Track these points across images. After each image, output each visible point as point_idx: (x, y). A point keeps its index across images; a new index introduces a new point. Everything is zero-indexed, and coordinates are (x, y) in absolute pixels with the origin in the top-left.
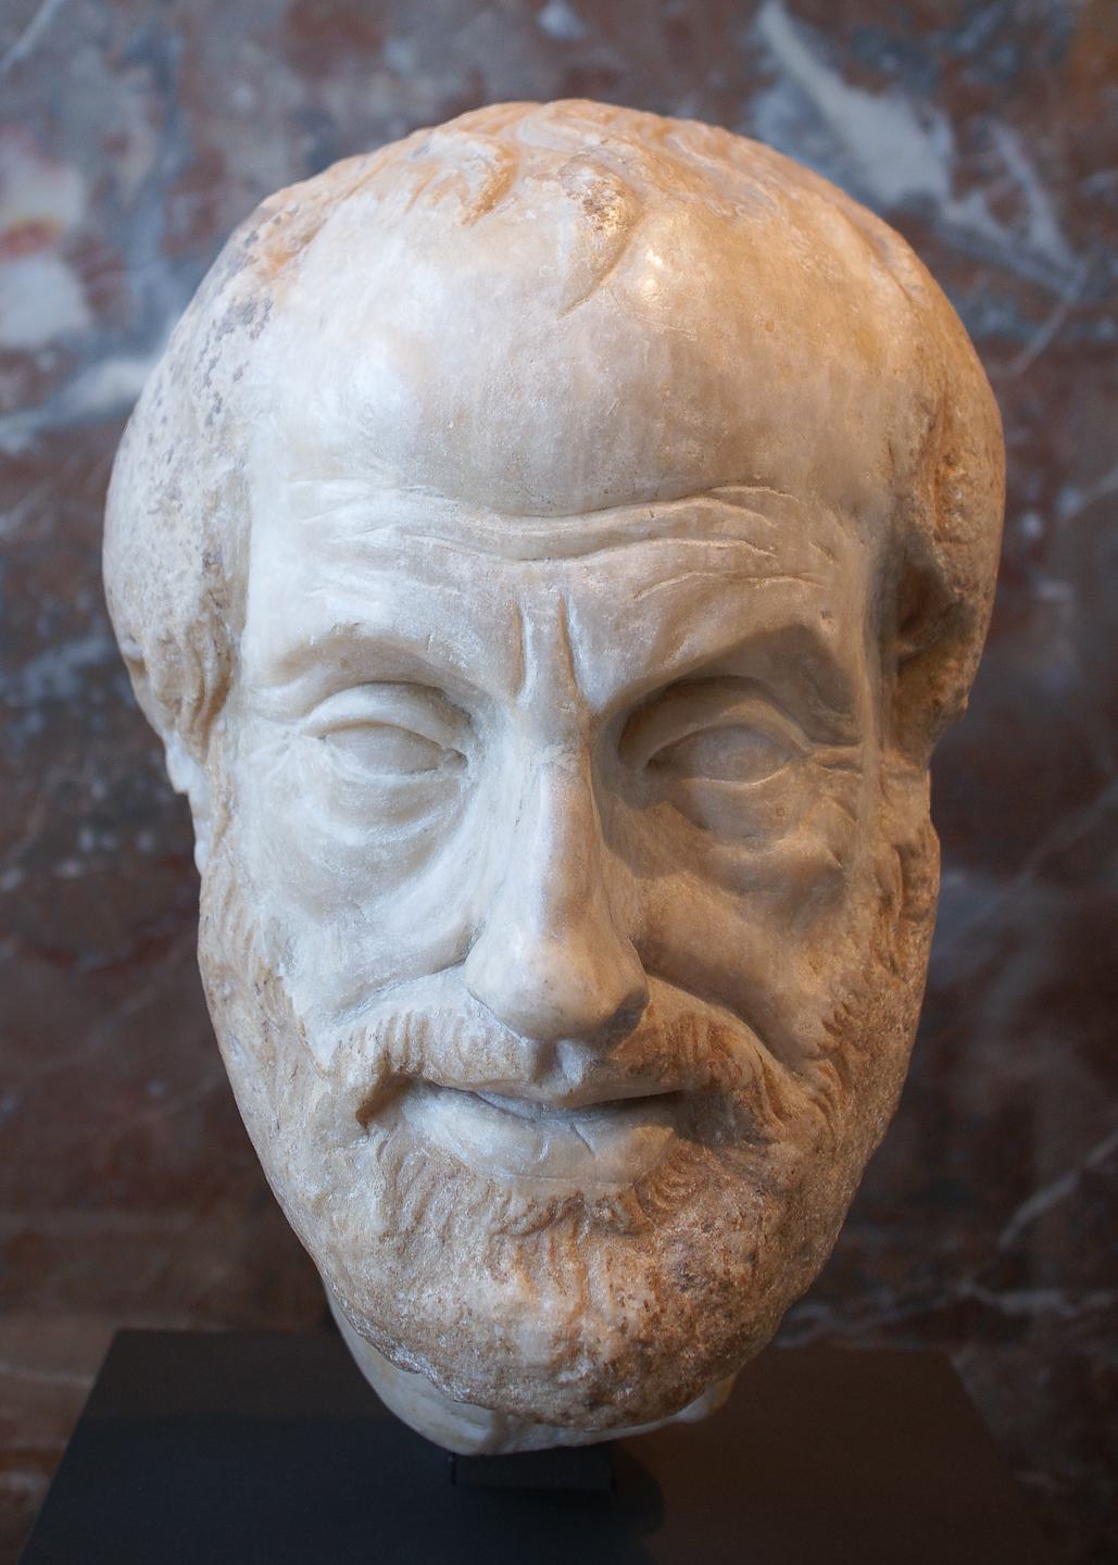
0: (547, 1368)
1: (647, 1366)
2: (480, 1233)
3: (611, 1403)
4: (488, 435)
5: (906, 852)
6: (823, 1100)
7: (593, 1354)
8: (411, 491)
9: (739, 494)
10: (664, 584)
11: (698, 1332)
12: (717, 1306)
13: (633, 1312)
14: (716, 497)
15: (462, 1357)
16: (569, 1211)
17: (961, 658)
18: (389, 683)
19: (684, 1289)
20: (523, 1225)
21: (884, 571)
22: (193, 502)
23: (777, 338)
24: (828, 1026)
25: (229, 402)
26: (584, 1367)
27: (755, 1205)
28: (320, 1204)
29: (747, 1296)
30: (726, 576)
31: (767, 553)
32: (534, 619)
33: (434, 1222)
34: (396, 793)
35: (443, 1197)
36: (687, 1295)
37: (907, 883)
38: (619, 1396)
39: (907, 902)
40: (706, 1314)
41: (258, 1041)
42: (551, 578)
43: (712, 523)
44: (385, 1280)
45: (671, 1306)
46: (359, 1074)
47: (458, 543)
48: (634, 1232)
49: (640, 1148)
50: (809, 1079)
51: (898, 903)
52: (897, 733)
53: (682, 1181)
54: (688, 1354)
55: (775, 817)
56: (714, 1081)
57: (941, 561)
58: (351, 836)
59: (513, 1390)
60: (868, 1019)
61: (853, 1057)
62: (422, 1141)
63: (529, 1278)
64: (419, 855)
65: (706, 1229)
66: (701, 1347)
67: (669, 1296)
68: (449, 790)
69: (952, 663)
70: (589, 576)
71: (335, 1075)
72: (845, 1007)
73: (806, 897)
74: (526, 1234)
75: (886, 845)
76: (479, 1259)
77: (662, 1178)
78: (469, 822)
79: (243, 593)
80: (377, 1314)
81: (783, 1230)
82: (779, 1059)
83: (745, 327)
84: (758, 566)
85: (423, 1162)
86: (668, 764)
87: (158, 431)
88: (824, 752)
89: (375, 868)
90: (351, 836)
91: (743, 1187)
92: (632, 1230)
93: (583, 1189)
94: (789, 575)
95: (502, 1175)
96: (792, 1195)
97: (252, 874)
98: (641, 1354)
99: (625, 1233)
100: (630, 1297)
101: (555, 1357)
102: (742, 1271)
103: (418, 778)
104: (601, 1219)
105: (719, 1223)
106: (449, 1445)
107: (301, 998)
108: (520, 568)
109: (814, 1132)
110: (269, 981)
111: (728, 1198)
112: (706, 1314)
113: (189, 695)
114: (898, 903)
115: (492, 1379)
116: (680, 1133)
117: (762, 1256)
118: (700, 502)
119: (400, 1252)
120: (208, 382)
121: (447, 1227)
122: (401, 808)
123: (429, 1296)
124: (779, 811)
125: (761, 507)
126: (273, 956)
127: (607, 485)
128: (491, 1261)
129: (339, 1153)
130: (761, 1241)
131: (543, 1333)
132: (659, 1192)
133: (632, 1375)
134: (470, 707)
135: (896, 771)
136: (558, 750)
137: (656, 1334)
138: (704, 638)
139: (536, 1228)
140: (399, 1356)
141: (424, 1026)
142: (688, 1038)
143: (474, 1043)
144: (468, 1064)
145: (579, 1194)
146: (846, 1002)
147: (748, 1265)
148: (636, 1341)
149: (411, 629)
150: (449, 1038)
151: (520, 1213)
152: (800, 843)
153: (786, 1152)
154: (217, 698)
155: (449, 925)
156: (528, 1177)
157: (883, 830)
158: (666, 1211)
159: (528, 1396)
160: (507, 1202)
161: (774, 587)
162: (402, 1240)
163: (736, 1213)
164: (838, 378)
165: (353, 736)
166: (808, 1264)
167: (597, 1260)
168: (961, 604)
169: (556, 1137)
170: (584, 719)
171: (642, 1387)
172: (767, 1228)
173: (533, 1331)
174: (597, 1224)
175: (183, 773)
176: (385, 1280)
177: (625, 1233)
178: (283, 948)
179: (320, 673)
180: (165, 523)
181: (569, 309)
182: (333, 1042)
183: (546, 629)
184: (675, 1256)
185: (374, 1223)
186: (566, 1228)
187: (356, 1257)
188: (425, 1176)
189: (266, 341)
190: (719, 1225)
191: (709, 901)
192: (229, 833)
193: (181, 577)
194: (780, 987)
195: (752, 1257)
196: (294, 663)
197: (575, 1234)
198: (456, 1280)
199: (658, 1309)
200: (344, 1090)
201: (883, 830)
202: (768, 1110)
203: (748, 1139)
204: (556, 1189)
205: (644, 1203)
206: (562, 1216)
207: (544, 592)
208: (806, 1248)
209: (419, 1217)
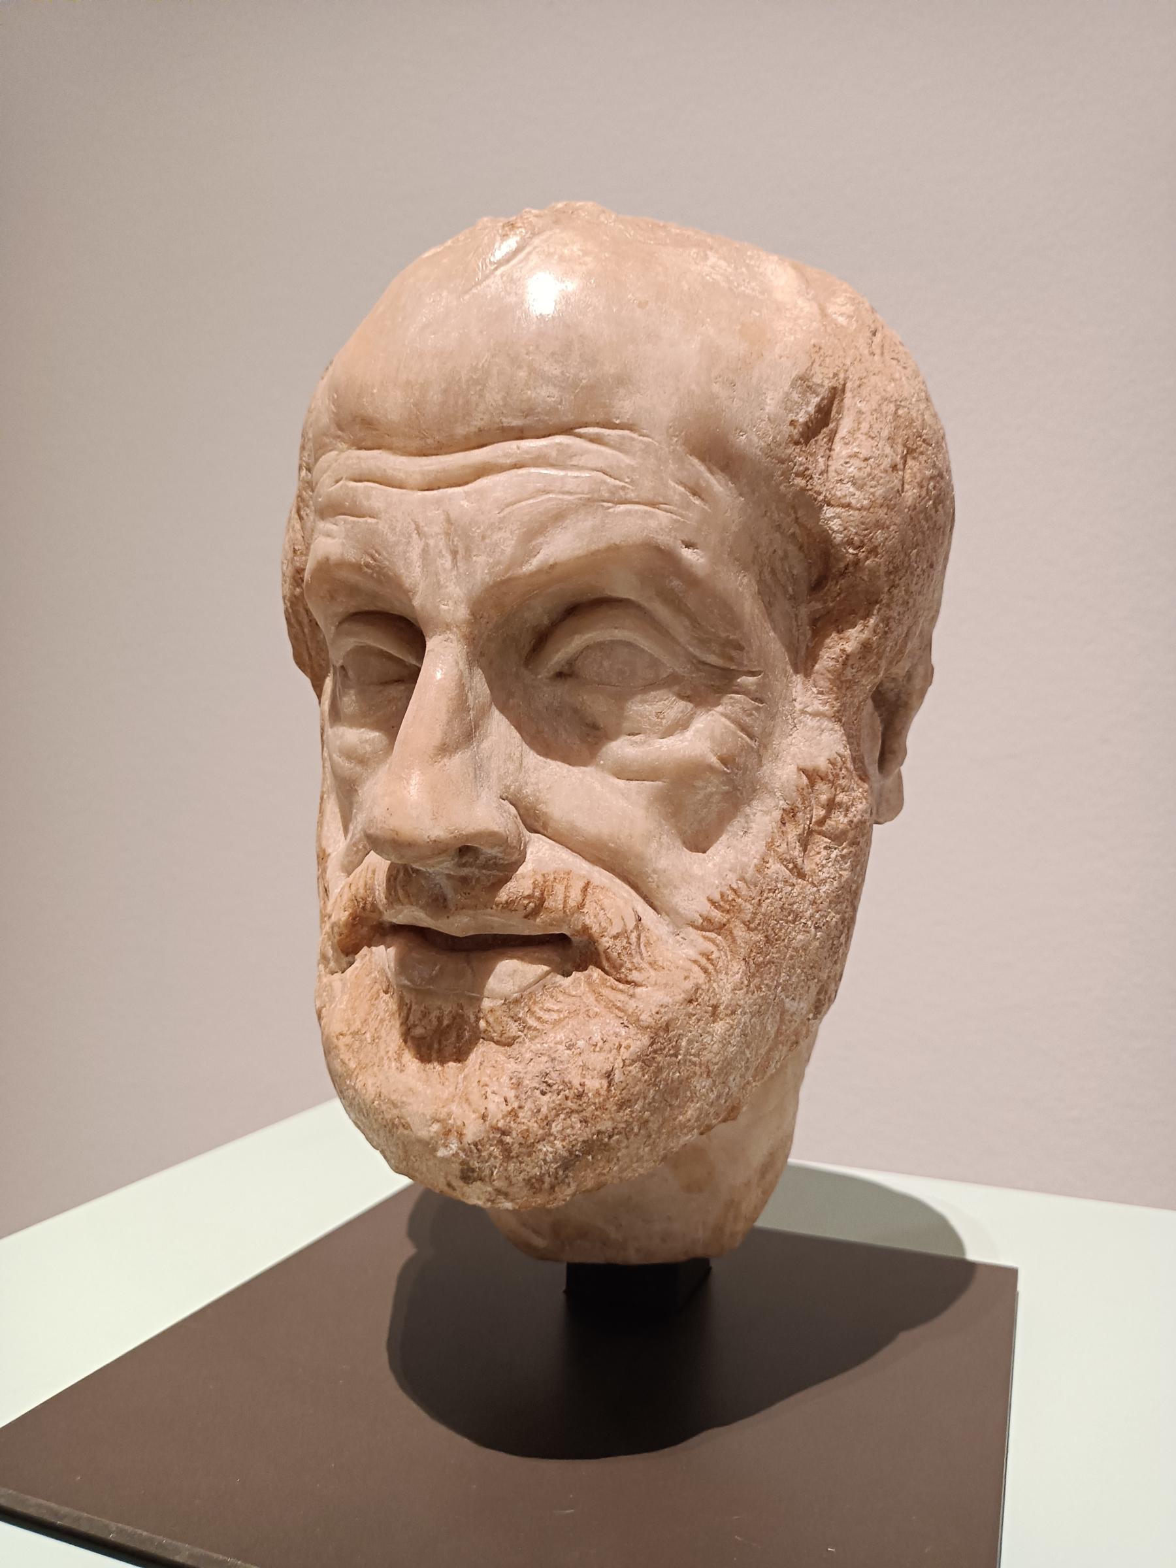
7: (461, 1135)
12: (572, 1111)
14: (580, 436)
19: (543, 1093)
27: (617, 1035)
31: (622, 484)
36: (545, 1098)
45: (529, 1105)
54: (545, 1148)
55: (655, 719)
60: (759, 904)
65: (568, 1048)
66: (558, 1144)
67: (529, 1097)
75: (793, 768)
77: (535, 1003)
84: (613, 493)
92: (503, 1039)
98: (501, 1142)
100: (494, 1093)
102: (597, 1085)
109: (688, 985)
112: (562, 1116)
117: (618, 1076)
125: (619, 447)
130: (619, 1064)
146: (735, 886)
147: (605, 1083)
158: (536, 1029)
161: (629, 513)
163: (597, 1038)
191: (597, 786)
199: (516, 1105)
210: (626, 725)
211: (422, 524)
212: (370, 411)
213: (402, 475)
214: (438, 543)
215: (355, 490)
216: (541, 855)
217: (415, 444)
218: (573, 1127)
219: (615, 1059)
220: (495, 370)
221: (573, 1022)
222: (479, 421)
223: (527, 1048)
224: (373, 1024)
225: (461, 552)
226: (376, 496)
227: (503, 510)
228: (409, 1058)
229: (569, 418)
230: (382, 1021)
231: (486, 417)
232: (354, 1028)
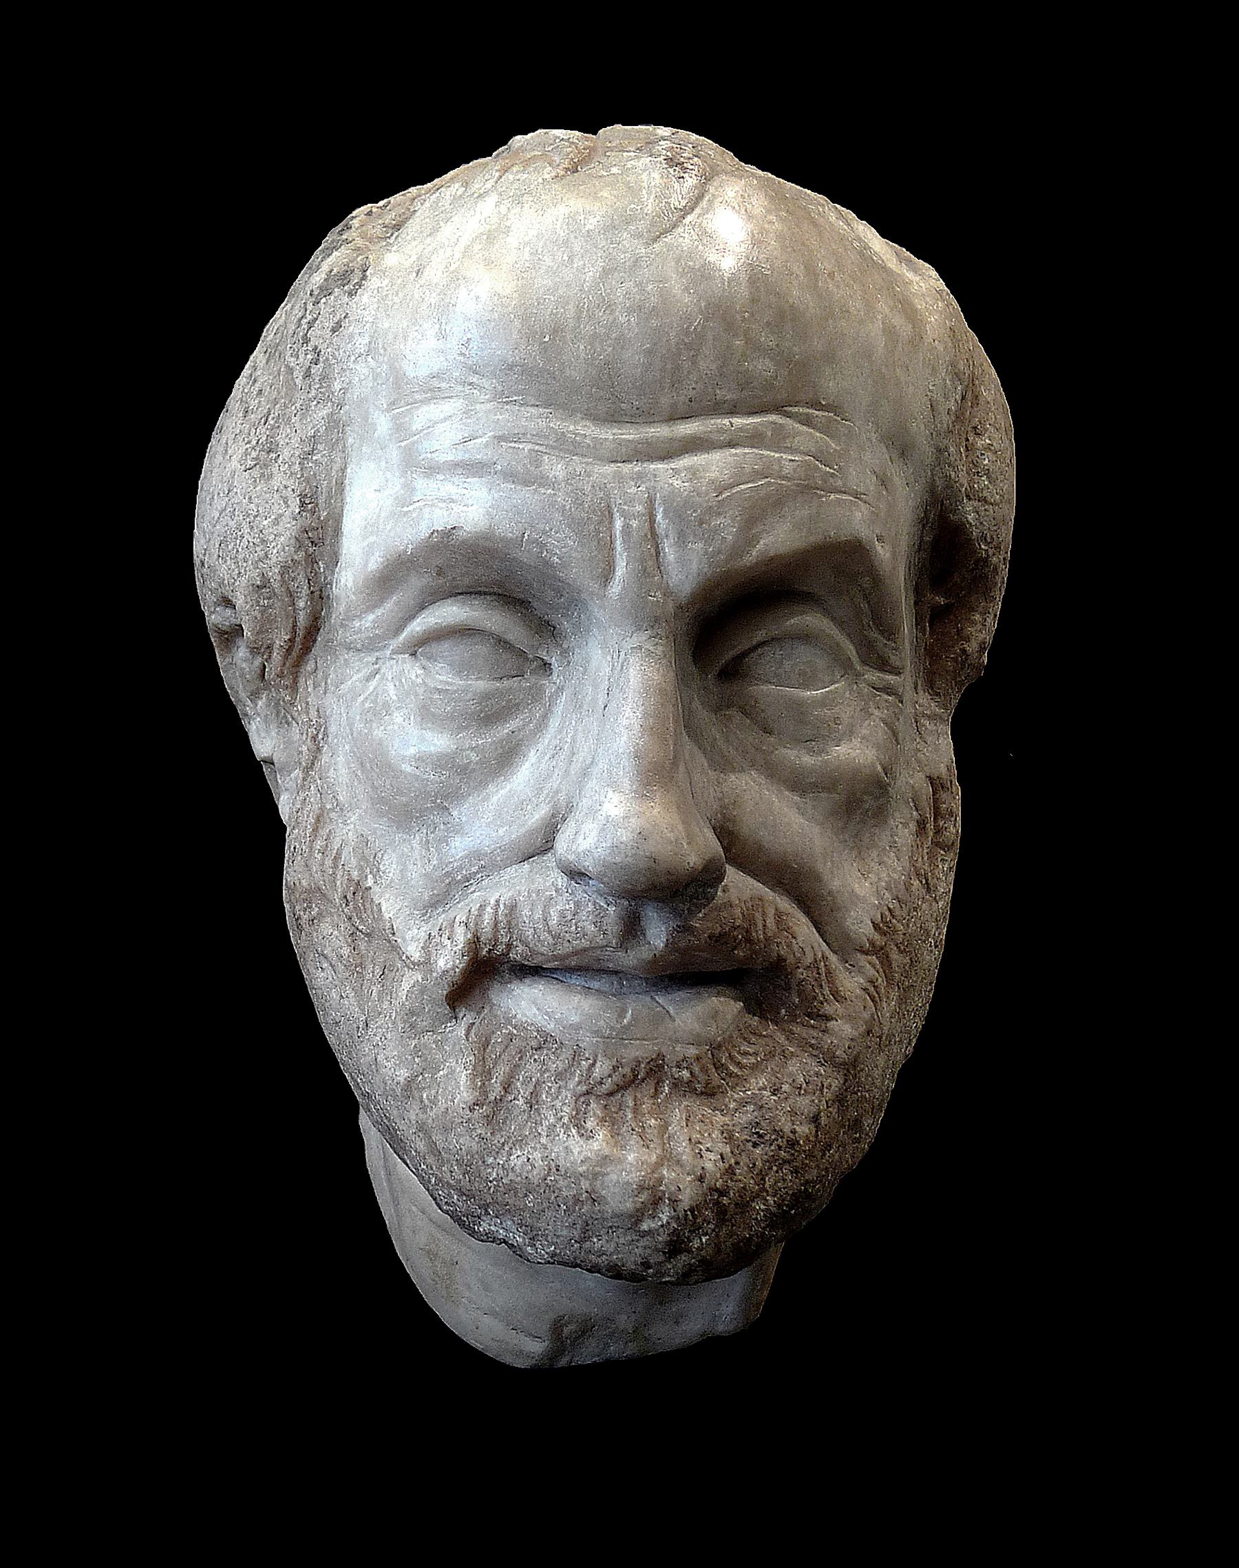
0: (632, 1216)
1: (722, 1213)
2: (567, 1095)
3: (689, 1251)
4: (582, 347)
5: (936, 783)
6: (873, 994)
7: (674, 1202)
8: (507, 403)
9: (807, 414)
10: (743, 487)
11: (767, 1185)
12: (785, 1162)
13: (710, 1163)
14: (788, 415)
15: (549, 1214)
16: (650, 1073)
17: (985, 613)
18: (479, 593)
19: (755, 1145)
20: (608, 1085)
21: (923, 522)
22: (290, 445)
23: (838, 287)
24: (876, 926)
25: (326, 351)
26: (665, 1216)
27: (817, 1074)
28: (410, 1087)
29: (810, 1155)
30: (798, 485)
32: (624, 514)
33: (522, 1091)
34: (486, 696)
35: (531, 1068)
37: (937, 814)
38: (696, 1244)
39: (938, 831)
40: (775, 1168)
41: (346, 951)
42: (639, 478)
43: (784, 438)
44: (475, 1147)
45: (744, 1159)
46: (450, 959)
47: (553, 448)
48: (709, 1093)
49: (715, 1015)
50: (861, 971)
51: (930, 826)
52: (930, 682)
53: (751, 1051)
56: (781, 959)
57: (971, 517)
58: (439, 742)
59: (596, 1243)
61: (895, 956)
62: (508, 1021)
63: (615, 1134)
64: (506, 757)
68: (536, 694)
69: (977, 617)
70: (670, 476)
71: (426, 964)
72: (889, 909)
73: (858, 804)
74: (611, 1094)
76: (566, 1120)
78: (554, 723)
79: (337, 531)
80: (465, 1183)
81: (840, 1099)
82: (835, 952)
83: (811, 271)
85: (511, 1038)
86: (733, 672)
87: (253, 403)
88: (873, 676)
89: (464, 771)
90: (439, 742)
91: (806, 1058)
93: (664, 1050)
94: (850, 495)
95: (587, 1040)
96: (850, 1067)
97: (341, 798)
98: (717, 1203)
99: (702, 1093)
100: (708, 1150)
101: (638, 1205)
103: (506, 683)
104: (680, 1079)
105: (786, 1087)
106: (508, 1359)
107: (390, 906)
108: (610, 469)
109: (866, 1015)
110: (358, 893)
111: (793, 1067)
112: (775, 1168)
113: (280, 638)
114: (930, 826)
115: (576, 1233)
116: (749, 1009)
117: (823, 1120)
118: (773, 417)
119: (489, 1120)
120: (306, 340)
121: (535, 1094)
122: (489, 713)
123: (517, 1159)
124: (837, 720)
125: (826, 430)
126: (361, 869)
127: (692, 393)
128: (578, 1121)
129: (428, 1038)
130: (823, 1106)
131: (628, 1183)
132: (731, 1057)
133: (709, 1223)
134: (555, 618)
135: (928, 712)
136: (644, 636)
137: (730, 1183)
138: (779, 538)
139: (620, 1088)
140: (484, 1227)
141: (513, 908)
142: (758, 916)
143: (562, 915)
144: (556, 937)
145: (660, 1056)
147: (812, 1126)
148: (713, 1189)
149: (507, 528)
150: (538, 915)
151: (606, 1074)
152: (855, 751)
153: (843, 1031)
154: (307, 639)
155: (537, 815)
156: (612, 1041)
157: (918, 761)
159: (611, 1247)
160: (593, 1065)
161: (838, 501)
162: (492, 1108)
164: (890, 332)
165: (446, 646)
166: (858, 1141)
167: (677, 1115)
168: (986, 561)
169: (636, 1006)
170: (670, 607)
171: (717, 1236)
172: (828, 1094)
173: (618, 1182)
174: (676, 1085)
175: (263, 742)
176: (475, 1147)
177: (702, 1093)
178: (370, 862)
179: (416, 583)
180: (263, 475)
181: (655, 240)
182: (423, 935)
183: (634, 523)
184: (748, 1115)
185: (465, 1094)
186: (648, 1088)
187: (446, 1130)
188: (512, 1050)
189: (364, 297)
190: (786, 1090)
192: (317, 765)
193: (276, 522)
194: (835, 884)
195: (815, 1119)
196: (386, 580)
197: (657, 1093)
198: (543, 1140)
199: (733, 1161)
200: (434, 974)
201: (918, 761)
202: (827, 991)
203: (810, 1016)
204: (636, 1051)
205: (719, 1066)
206: (647, 1076)
207: (633, 490)
208: (856, 1124)
209: (507, 1087)
216: (739, 885)
218: (784, 1180)
219: (820, 1101)
220: (710, 336)
221: (771, 1065)
223: (733, 1097)
227: (721, 493)
229: (782, 395)
231: (700, 386)
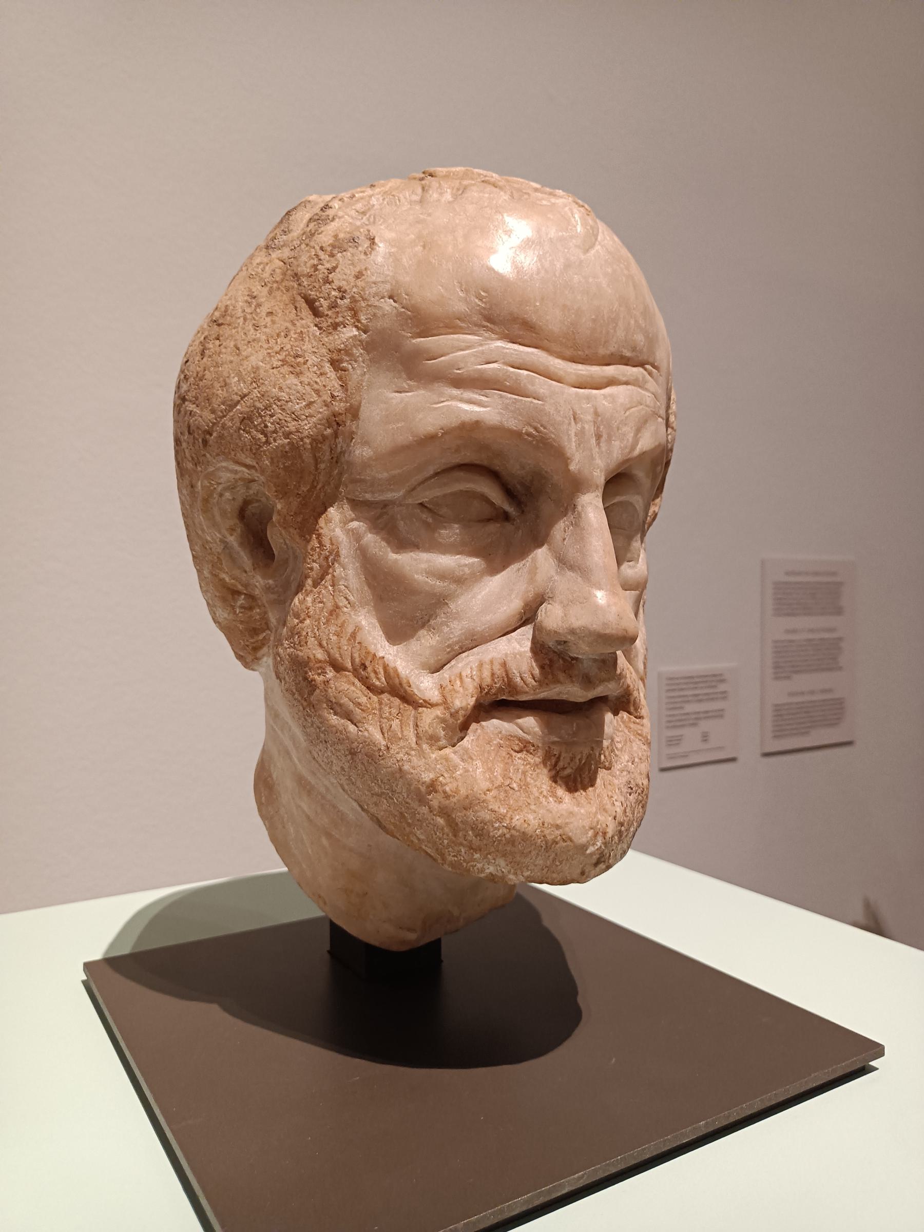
14: (646, 369)
36: (631, 797)
210: (629, 555)
211: (579, 412)
212: (534, 318)
213: (561, 373)
214: (590, 428)
215: (519, 374)
217: (568, 353)
222: (612, 348)
224: (517, 777)
225: (605, 436)
226: (541, 385)
228: (561, 792)
230: (524, 773)
232: (498, 783)
